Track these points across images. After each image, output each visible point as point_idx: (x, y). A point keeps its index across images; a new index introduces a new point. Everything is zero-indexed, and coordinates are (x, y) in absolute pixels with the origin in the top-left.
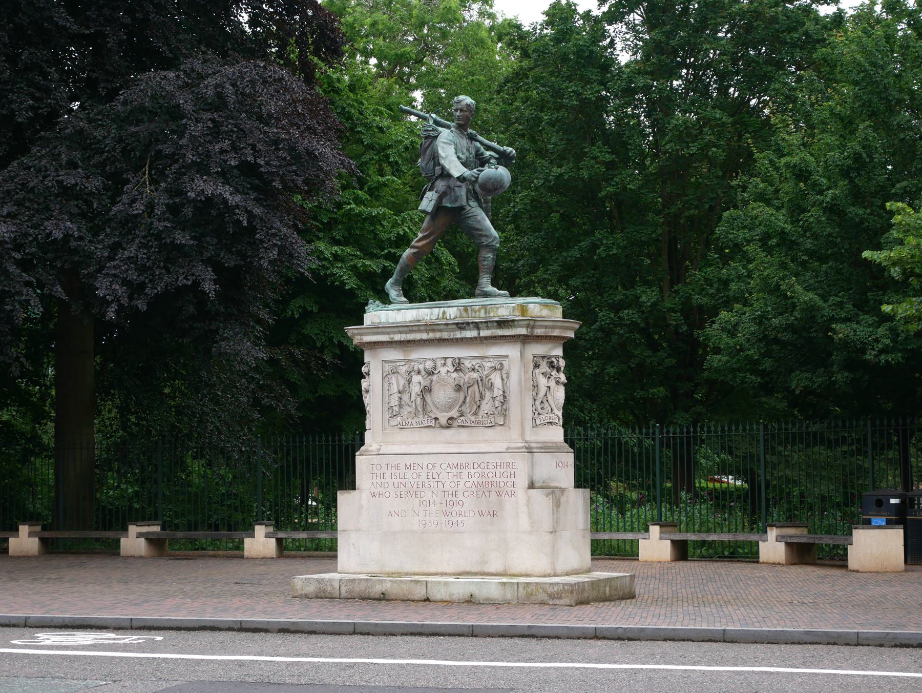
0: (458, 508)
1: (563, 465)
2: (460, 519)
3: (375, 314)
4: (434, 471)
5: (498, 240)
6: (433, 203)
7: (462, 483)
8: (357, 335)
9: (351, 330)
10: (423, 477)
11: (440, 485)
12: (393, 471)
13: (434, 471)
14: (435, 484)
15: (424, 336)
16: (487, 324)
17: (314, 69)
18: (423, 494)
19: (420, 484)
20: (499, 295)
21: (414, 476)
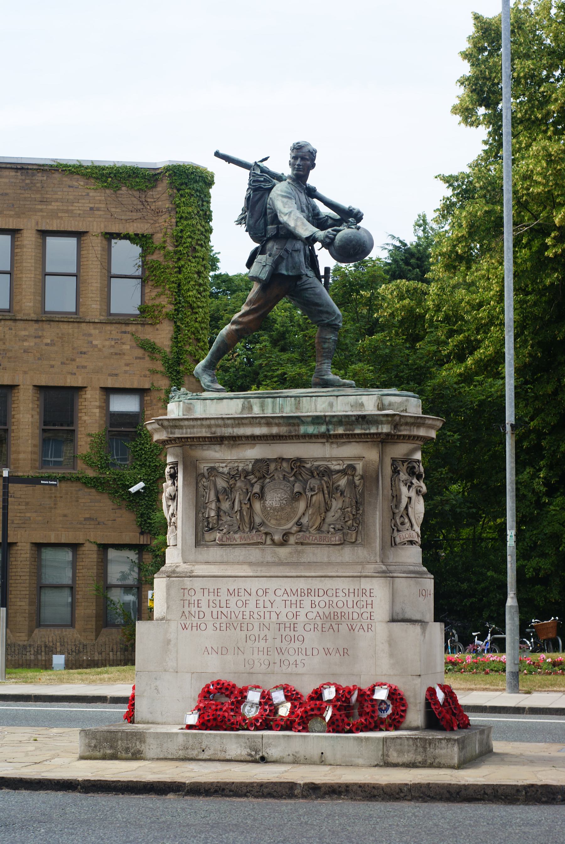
0: (297, 644)
1: (422, 593)
2: (299, 658)
4: (266, 599)
5: (341, 318)
6: (267, 268)
7: (302, 613)
10: (251, 605)
11: (274, 616)
12: (212, 597)
13: (266, 599)
14: (267, 615)
15: (258, 431)
16: (342, 420)
18: (250, 627)
19: (247, 614)
21: (240, 604)
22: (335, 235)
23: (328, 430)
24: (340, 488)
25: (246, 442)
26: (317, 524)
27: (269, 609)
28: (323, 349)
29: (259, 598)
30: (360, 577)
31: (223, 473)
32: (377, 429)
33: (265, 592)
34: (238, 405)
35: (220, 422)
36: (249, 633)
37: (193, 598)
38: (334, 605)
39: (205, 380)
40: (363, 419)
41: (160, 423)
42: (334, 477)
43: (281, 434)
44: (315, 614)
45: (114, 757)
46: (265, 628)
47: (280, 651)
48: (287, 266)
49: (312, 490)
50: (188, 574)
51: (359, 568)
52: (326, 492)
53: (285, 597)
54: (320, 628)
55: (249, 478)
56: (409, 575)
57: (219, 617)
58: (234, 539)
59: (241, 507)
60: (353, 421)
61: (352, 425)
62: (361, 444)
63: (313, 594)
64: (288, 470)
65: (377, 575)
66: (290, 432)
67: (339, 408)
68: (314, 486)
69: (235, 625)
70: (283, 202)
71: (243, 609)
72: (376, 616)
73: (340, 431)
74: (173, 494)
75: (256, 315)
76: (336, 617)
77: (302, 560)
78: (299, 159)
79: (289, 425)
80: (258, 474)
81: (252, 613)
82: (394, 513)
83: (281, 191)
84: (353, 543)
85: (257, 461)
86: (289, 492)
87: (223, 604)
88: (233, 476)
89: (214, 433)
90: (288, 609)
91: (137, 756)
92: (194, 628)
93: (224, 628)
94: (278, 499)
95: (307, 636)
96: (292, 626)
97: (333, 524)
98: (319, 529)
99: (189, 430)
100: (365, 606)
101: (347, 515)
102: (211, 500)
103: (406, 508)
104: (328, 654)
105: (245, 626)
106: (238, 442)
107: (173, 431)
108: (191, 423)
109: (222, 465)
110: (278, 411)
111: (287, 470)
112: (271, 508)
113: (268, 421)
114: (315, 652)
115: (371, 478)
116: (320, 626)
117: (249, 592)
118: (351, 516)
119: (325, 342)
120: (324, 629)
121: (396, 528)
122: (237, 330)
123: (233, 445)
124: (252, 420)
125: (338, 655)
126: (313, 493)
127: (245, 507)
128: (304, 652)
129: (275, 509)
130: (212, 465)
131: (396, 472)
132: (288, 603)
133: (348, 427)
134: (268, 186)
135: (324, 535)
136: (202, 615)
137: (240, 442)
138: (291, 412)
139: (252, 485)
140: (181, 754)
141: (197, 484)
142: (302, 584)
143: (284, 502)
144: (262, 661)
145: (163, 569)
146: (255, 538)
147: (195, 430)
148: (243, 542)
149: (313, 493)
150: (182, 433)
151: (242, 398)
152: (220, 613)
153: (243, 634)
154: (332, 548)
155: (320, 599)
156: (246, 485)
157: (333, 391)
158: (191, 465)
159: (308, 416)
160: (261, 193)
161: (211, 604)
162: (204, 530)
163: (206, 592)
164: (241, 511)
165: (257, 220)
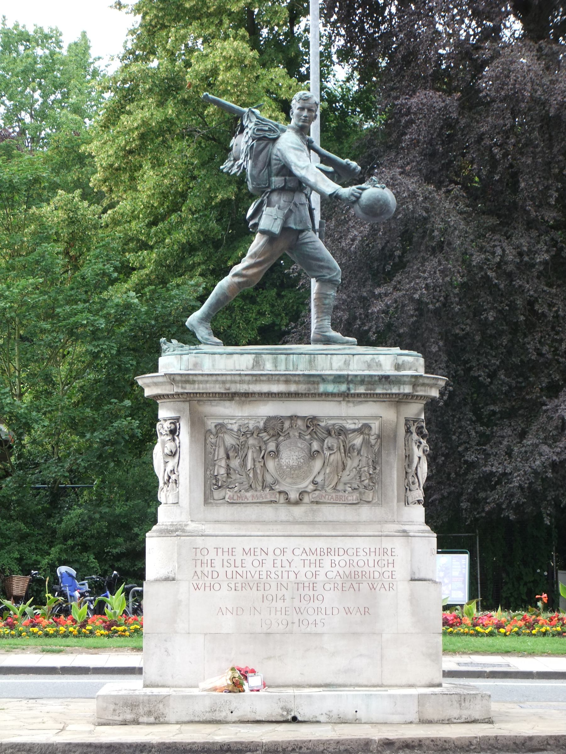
0: (317, 603)
2: (318, 618)
3: (173, 360)
4: (284, 558)
7: (322, 572)
8: (149, 385)
9: (141, 380)
10: (268, 565)
11: (292, 576)
12: (226, 557)
13: (284, 558)
14: (285, 575)
15: (275, 388)
16: (363, 380)
17: (250, 40)
18: (267, 587)
19: (264, 573)
20: (347, 343)
21: (256, 563)
22: (361, 194)
23: (349, 389)
24: (355, 447)
25: (259, 399)
26: (334, 484)
27: (288, 568)
28: (324, 304)
29: (277, 558)
30: (381, 536)
31: (232, 430)
32: (399, 389)
33: (283, 552)
34: (249, 361)
35: (238, 378)
36: (266, 593)
37: (206, 557)
38: (355, 564)
39: (203, 332)
40: (386, 379)
41: (172, 377)
42: (350, 436)
43: (300, 392)
44: (335, 573)
45: (136, 722)
46: (282, 588)
47: (299, 611)
48: (295, 219)
49: (329, 448)
50: (200, 533)
51: (378, 527)
52: (342, 451)
53: (304, 556)
54: (340, 587)
55: (261, 435)
56: (423, 535)
57: (234, 577)
58: (246, 497)
59: (254, 465)
60: (375, 381)
61: (373, 384)
62: (378, 403)
63: (332, 553)
64: (303, 428)
65: (398, 534)
66: (309, 390)
67: (355, 367)
68: (333, 446)
69: (251, 585)
70: (296, 155)
71: (260, 568)
72: (397, 576)
73: (361, 390)
74: (174, 451)
75: (260, 268)
76: (357, 576)
77: (318, 519)
78: (306, 110)
79: (309, 383)
80: (271, 432)
81: (269, 573)
82: (406, 473)
83: (292, 143)
84: (369, 502)
85: (269, 419)
86: (306, 450)
87: (238, 563)
88: (245, 433)
89: (229, 389)
90: (307, 568)
91: (159, 721)
92: (208, 589)
93: (240, 588)
94: (295, 457)
95: (327, 595)
96: (311, 585)
97: (348, 483)
98: (335, 488)
99: (201, 386)
100: (386, 565)
101: (363, 474)
102: (220, 457)
103: (417, 468)
104: (349, 614)
105: (261, 586)
106: (249, 399)
107: (184, 385)
108: (206, 378)
109: (231, 421)
110: (291, 368)
111: (302, 428)
112: (287, 467)
113: (287, 379)
114: (335, 611)
115: (386, 438)
116: (340, 585)
117: (266, 551)
118: (368, 475)
119: (326, 298)
120: (344, 589)
121: (408, 488)
122: (239, 283)
123: (243, 402)
124: (271, 377)
125: (359, 614)
126: (331, 452)
127: (258, 465)
128: (323, 611)
129: (291, 468)
130: (221, 421)
131: (408, 431)
132: (307, 562)
133: (370, 386)
134: (273, 136)
135: (341, 494)
136: (215, 575)
137: (252, 399)
138: (306, 369)
139: (266, 443)
140: (208, 716)
141: (205, 440)
142: (321, 543)
143: (302, 461)
144: (279, 622)
145: (154, 528)
146: (268, 496)
147: (208, 385)
148: (255, 501)
149: (331, 452)
150: (194, 389)
151: (253, 354)
152: (234, 573)
153: (260, 594)
154: (349, 507)
155: (340, 558)
156: (259, 443)
157: (344, 349)
158: (197, 422)
159: (330, 375)
160: (266, 142)
161: (225, 563)
162: (214, 486)
163: (220, 551)
164: (254, 469)
165: (261, 170)
